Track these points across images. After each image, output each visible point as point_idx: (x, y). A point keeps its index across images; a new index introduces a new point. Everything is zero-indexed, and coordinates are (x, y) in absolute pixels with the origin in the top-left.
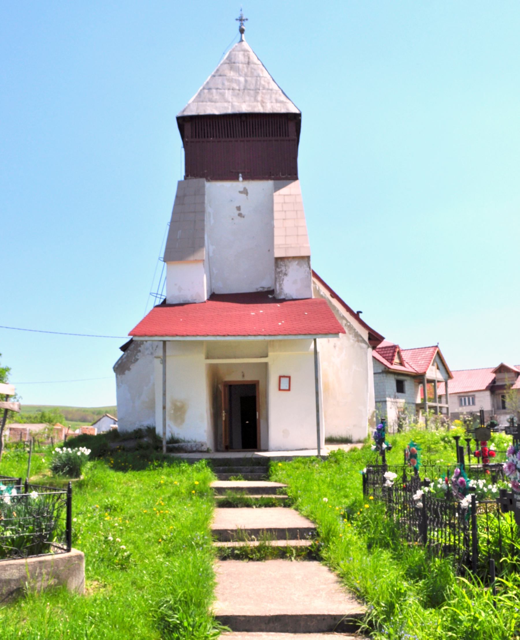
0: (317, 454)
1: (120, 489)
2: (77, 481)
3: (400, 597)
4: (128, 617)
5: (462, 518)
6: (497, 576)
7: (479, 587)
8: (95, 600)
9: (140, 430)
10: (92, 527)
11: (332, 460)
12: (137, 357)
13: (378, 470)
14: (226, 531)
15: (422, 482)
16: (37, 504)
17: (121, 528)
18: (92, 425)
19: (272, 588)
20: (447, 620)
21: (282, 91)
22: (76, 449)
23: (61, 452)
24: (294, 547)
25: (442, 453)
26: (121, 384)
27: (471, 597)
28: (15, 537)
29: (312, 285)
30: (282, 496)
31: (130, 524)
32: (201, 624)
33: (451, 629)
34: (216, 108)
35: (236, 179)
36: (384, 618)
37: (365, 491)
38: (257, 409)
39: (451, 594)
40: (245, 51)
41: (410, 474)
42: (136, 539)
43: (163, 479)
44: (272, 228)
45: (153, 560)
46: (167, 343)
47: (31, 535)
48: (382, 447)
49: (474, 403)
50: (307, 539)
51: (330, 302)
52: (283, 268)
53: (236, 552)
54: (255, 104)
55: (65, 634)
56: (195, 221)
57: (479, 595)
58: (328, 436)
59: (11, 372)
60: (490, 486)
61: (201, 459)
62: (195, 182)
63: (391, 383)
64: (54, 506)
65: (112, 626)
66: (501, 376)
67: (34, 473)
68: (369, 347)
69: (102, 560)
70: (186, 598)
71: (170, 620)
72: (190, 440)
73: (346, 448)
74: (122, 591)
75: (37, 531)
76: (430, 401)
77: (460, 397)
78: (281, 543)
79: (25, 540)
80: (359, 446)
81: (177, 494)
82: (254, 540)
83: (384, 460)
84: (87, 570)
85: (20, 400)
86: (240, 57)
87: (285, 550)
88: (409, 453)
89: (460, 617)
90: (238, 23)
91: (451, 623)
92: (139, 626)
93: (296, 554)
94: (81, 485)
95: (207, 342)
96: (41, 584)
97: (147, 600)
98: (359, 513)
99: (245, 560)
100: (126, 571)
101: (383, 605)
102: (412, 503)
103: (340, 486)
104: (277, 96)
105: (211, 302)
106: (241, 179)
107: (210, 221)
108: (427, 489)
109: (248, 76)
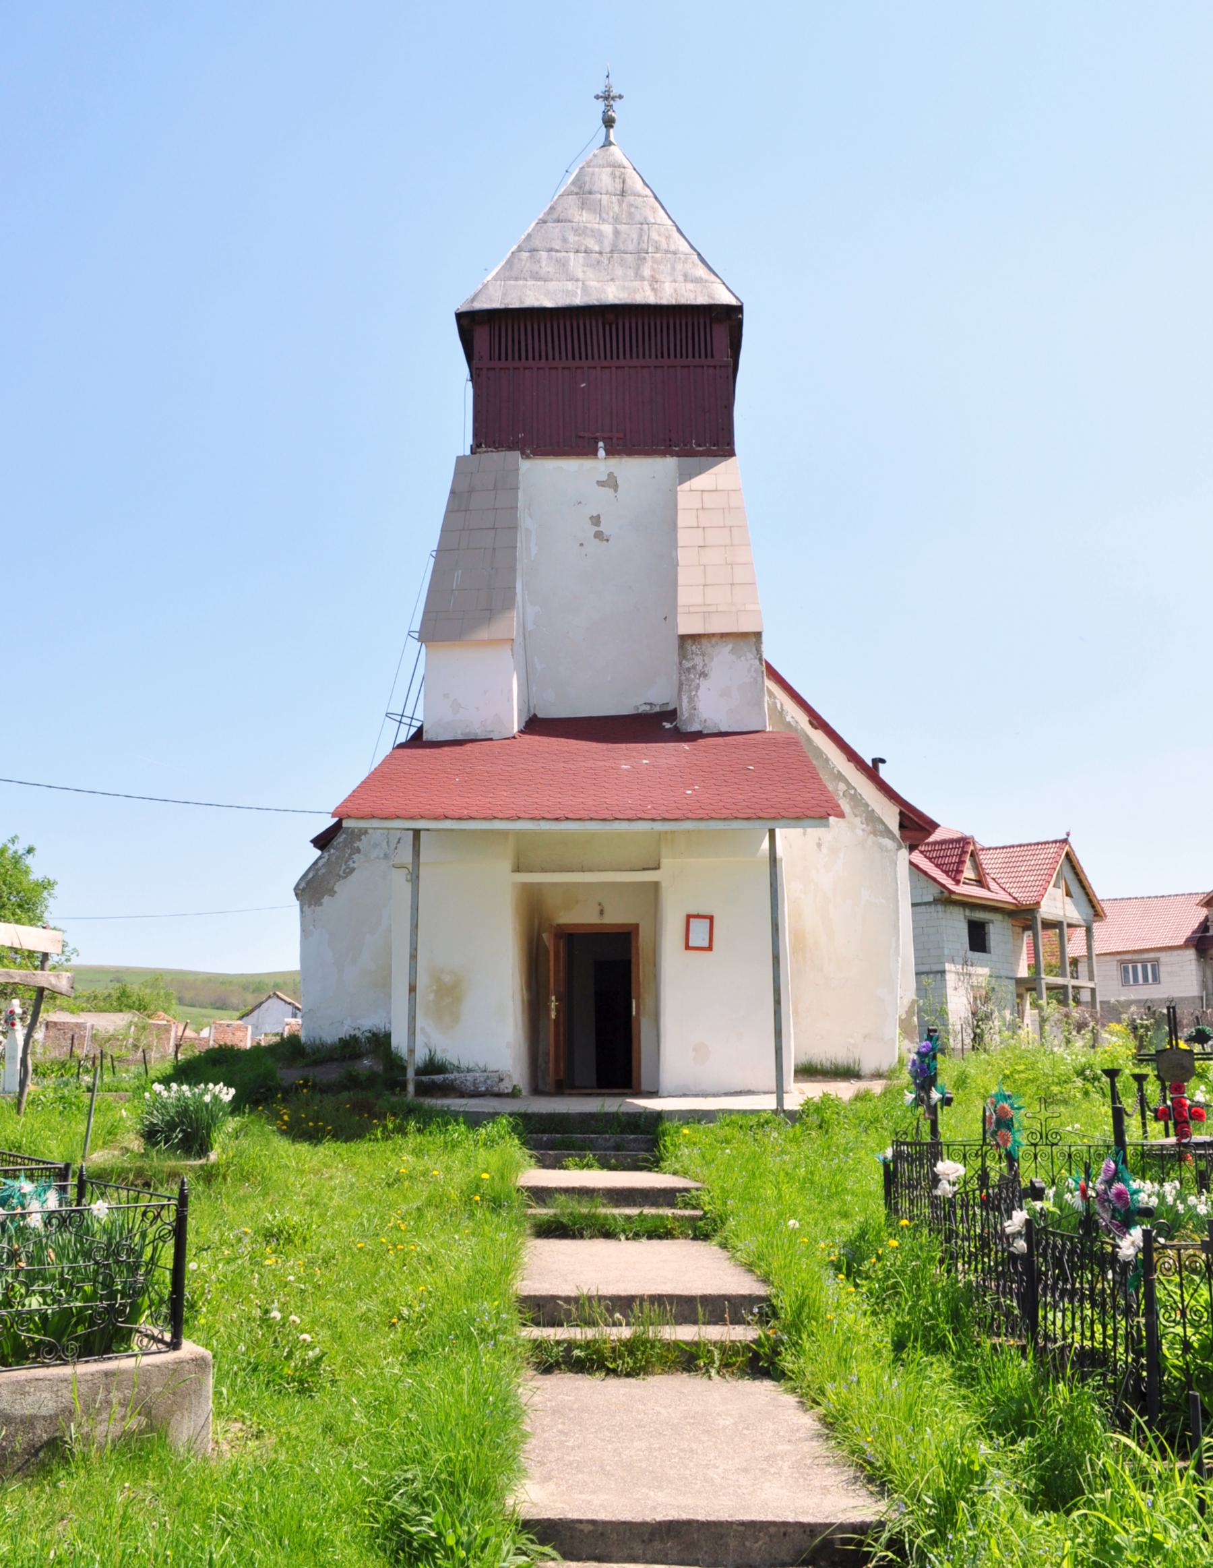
0: (774, 1107)
2: (202, 1167)
3: (971, 1483)
4: (313, 1518)
5: (1121, 1284)
7: (1164, 1459)
9: (354, 1038)
10: (233, 1283)
11: (813, 1120)
12: (351, 864)
14: (553, 1299)
16: (105, 1231)
17: (302, 1286)
18: (241, 1018)
19: (660, 1449)
21: (699, 255)
22: (202, 1086)
23: (165, 1094)
24: (715, 1344)
27: (1146, 1486)
28: (49, 1312)
29: (766, 698)
30: (688, 1212)
31: (323, 1275)
32: (487, 1540)
34: (547, 293)
35: (594, 453)
36: (931, 1535)
37: (892, 1207)
38: (633, 994)
39: (1095, 1476)
40: (616, 165)
41: (996, 1169)
42: (336, 1315)
45: (375, 1371)
46: (422, 833)
47: (87, 1308)
48: (929, 1098)
49: (1156, 979)
51: (809, 740)
52: (698, 660)
53: (577, 1352)
54: (637, 283)
55: (160, 1559)
57: (1165, 1480)
58: (803, 1059)
59: (56, 890)
60: (1192, 1200)
61: (498, 1114)
62: (495, 459)
63: (956, 926)
64: (144, 1235)
65: (273, 1542)
67: (100, 1143)
68: (900, 847)
69: (255, 1370)
70: (451, 1474)
71: (413, 1530)
72: (471, 1066)
73: (844, 1090)
74: (299, 1449)
76: (1050, 972)
77: (1122, 962)
78: (685, 1333)
79: (74, 1319)
80: (877, 1087)
81: (436, 1202)
82: (621, 1325)
83: (934, 1131)
84: (218, 1394)
86: (604, 180)
87: (694, 1349)
88: (994, 1117)
89: (1116, 1538)
90: (600, 105)
91: (1096, 1553)
92: (337, 1543)
93: (721, 1361)
94: (209, 1176)
95: (519, 834)
96: (106, 1429)
97: (359, 1473)
98: (874, 1260)
99: (597, 1375)
100: (311, 1396)
101: (930, 1502)
102: (1001, 1239)
103: (829, 1188)
104: (688, 266)
106: (602, 453)
107: (529, 550)
108: (1038, 1205)
109: (621, 223)
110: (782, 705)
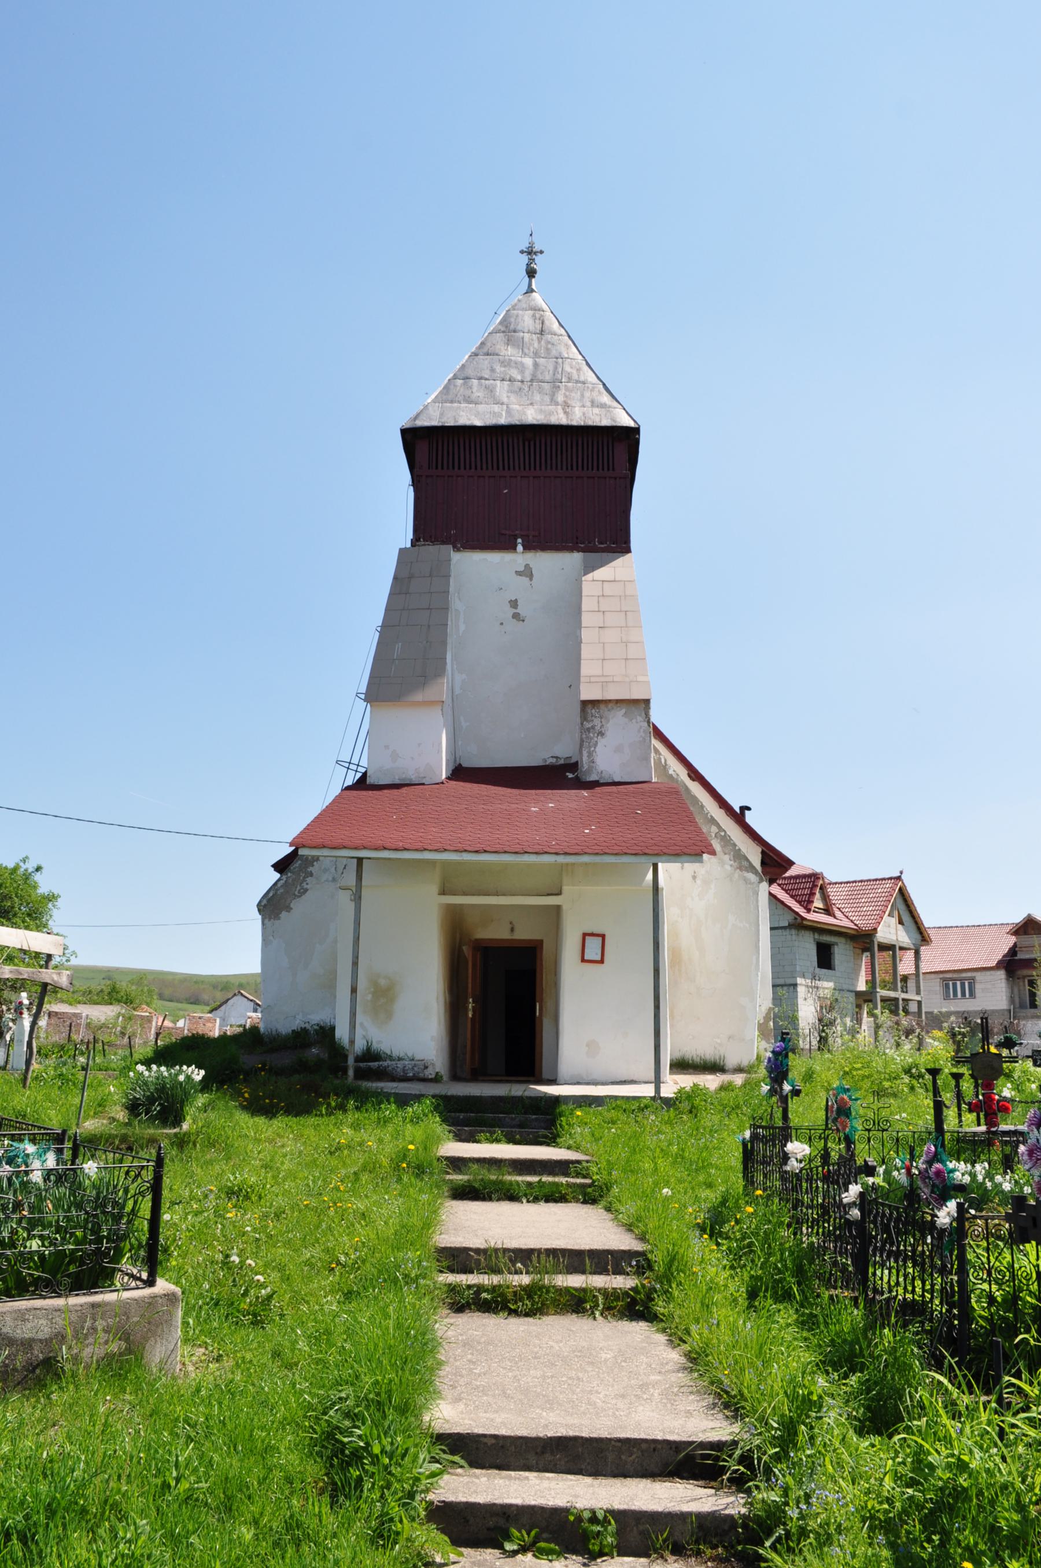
0: (653, 1094)
1: (259, 1153)
2: (176, 1134)
4: (262, 1428)
5: (938, 1247)
6: (1008, 1374)
7: (971, 1393)
8: (198, 1391)
9: (304, 1030)
11: (685, 1106)
13: (774, 1135)
14: (466, 1250)
15: (860, 1167)
16: (94, 1186)
18: (211, 1012)
19: (552, 1377)
20: (904, 1463)
21: (604, 385)
22: (178, 1067)
23: (146, 1073)
24: (599, 1290)
25: (906, 1099)
26: (271, 938)
27: (955, 1415)
28: (47, 1252)
29: (653, 754)
30: (579, 1181)
31: (275, 1227)
32: (407, 1450)
33: (912, 1483)
35: (513, 548)
36: (776, 1453)
37: (749, 1181)
38: (537, 998)
40: (537, 309)
42: (286, 1260)
43: (345, 1134)
44: (579, 642)
45: (317, 1307)
47: (78, 1250)
48: (782, 1089)
49: (972, 995)
50: (628, 1274)
51: (687, 789)
52: (597, 722)
53: (484, 1295)
56: (429, 626)
57: (972, 1412)
58: (678, 1055)
59: (60, 903)
60: (998, 1178)
62: (431, 551)
63: (807, 948)
64: (126, 1191)
65: (229, 1448)
66: (1026, 940)
67: (92, 1113)
68: (761, 881)
69: (217, 1304)
70: (378, 1394)
71: (346, 1440)
73: (711, 1082)
74: (252, 1371)
75: (91, 1243)
76: (884, 987)
77: (944, 980)
78: (575, 1281)
80: (738, 1079)
81: (370, 1167)
82: (521, 1273)
83: (785, 1117)
84: (186, 1324)
85: (72, 958)
86: (527, 321)
89: (930, 1458)
90: (525, 259)
91: (913, 1471)
93: (604, 1304)
94: (182, 1142)
96: (93, 1351)
98: (733, 1223)
99: (501, 1314)
102: (839, 1208)
103: (697, 1163)
105: (453, 783)
106: (520, 548)
107: (458, 626)
108: (870, 1180)
110: (665, 760)
